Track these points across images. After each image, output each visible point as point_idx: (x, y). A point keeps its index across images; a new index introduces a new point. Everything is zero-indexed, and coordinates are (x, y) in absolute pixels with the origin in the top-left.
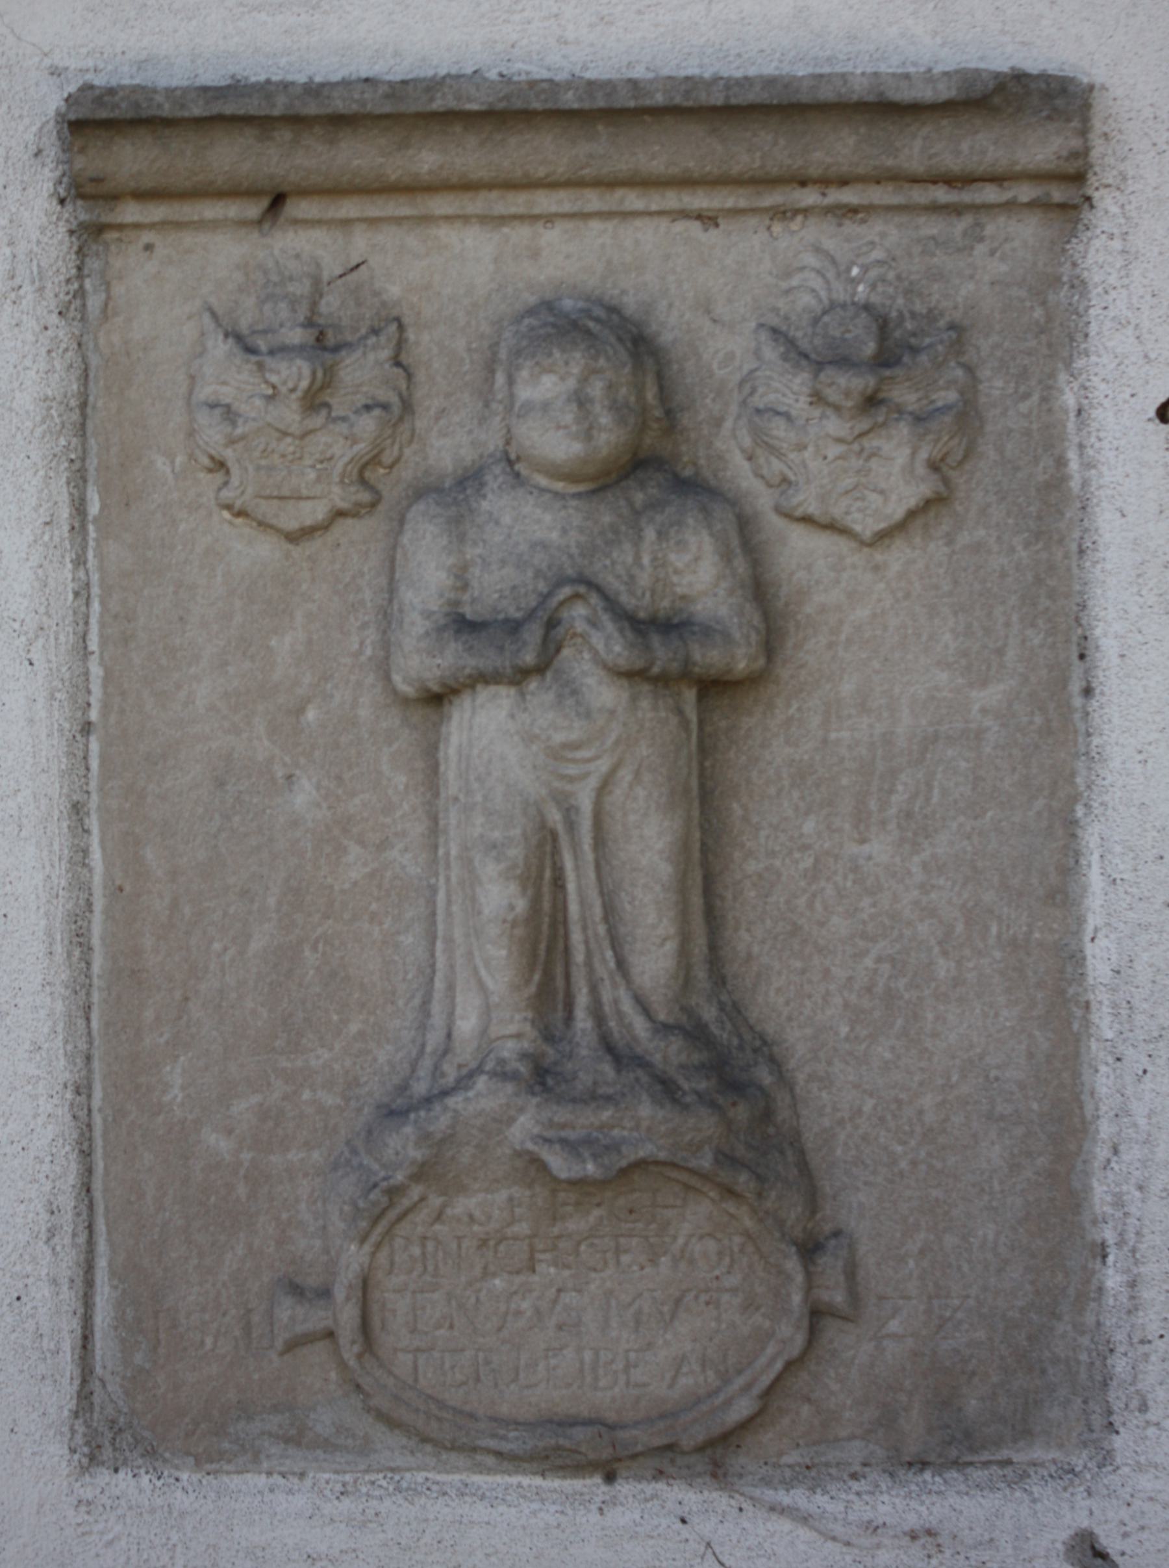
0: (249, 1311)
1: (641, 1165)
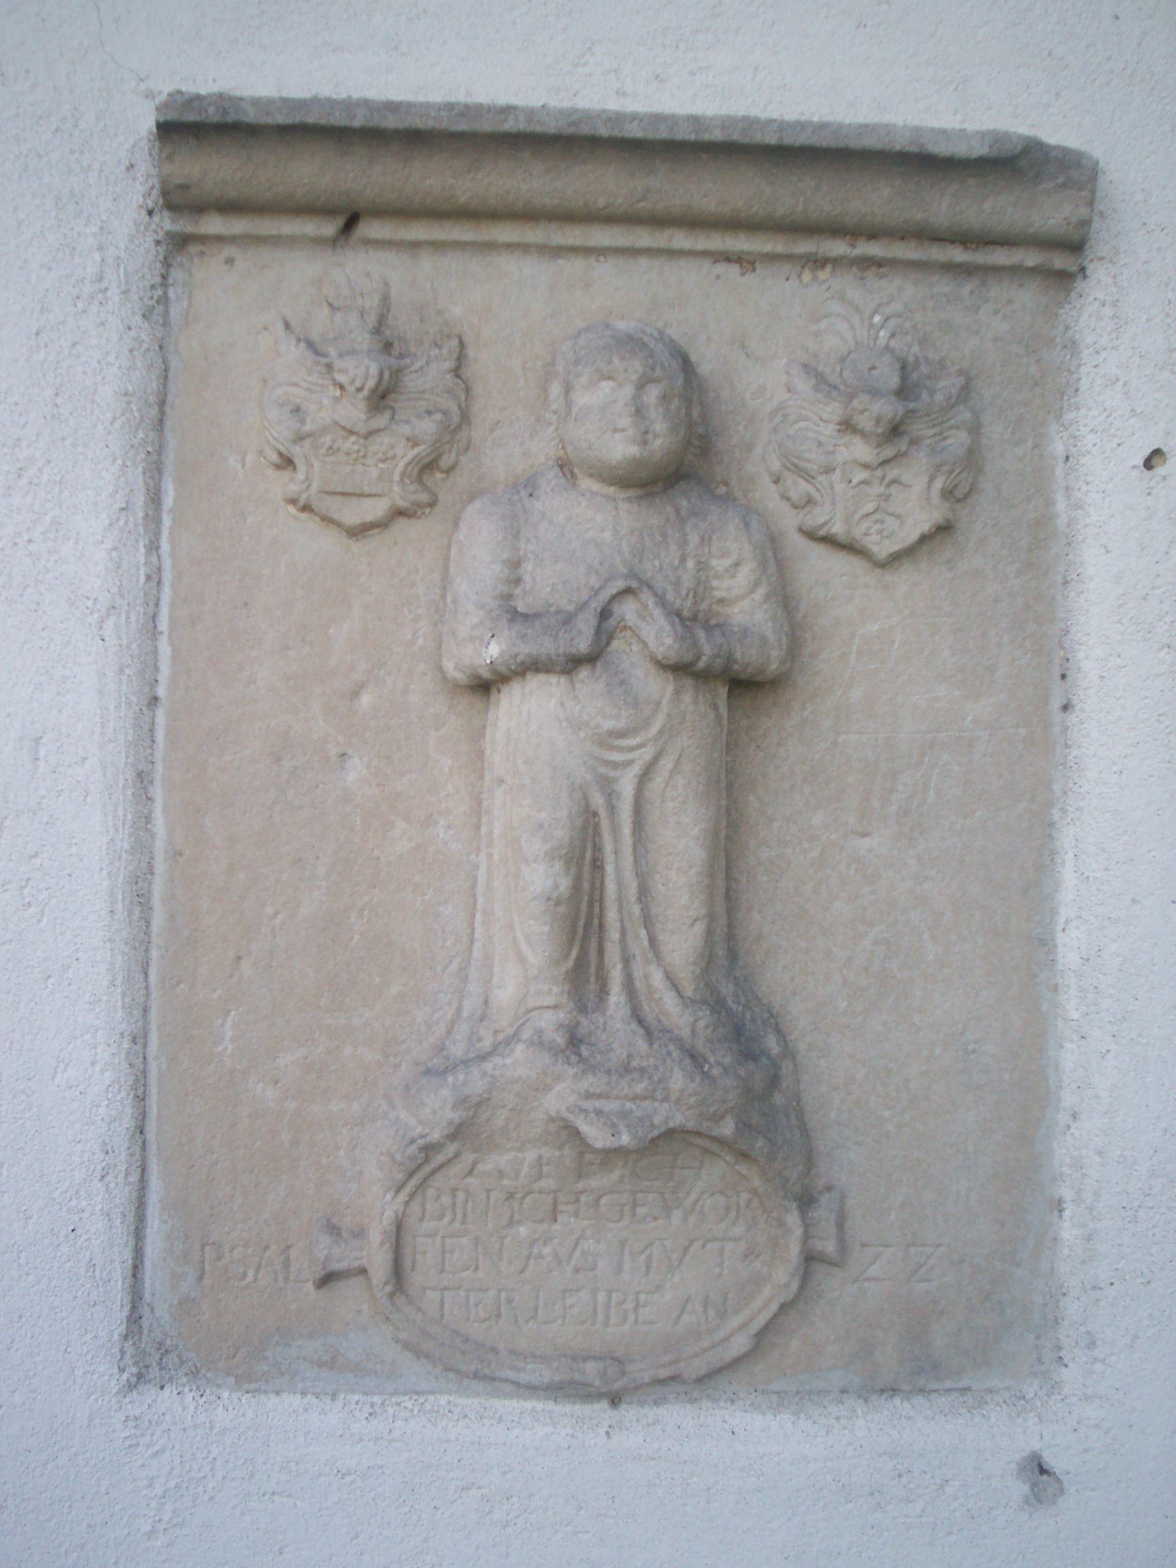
0: (288, 1247)
1: (670, 1133)
